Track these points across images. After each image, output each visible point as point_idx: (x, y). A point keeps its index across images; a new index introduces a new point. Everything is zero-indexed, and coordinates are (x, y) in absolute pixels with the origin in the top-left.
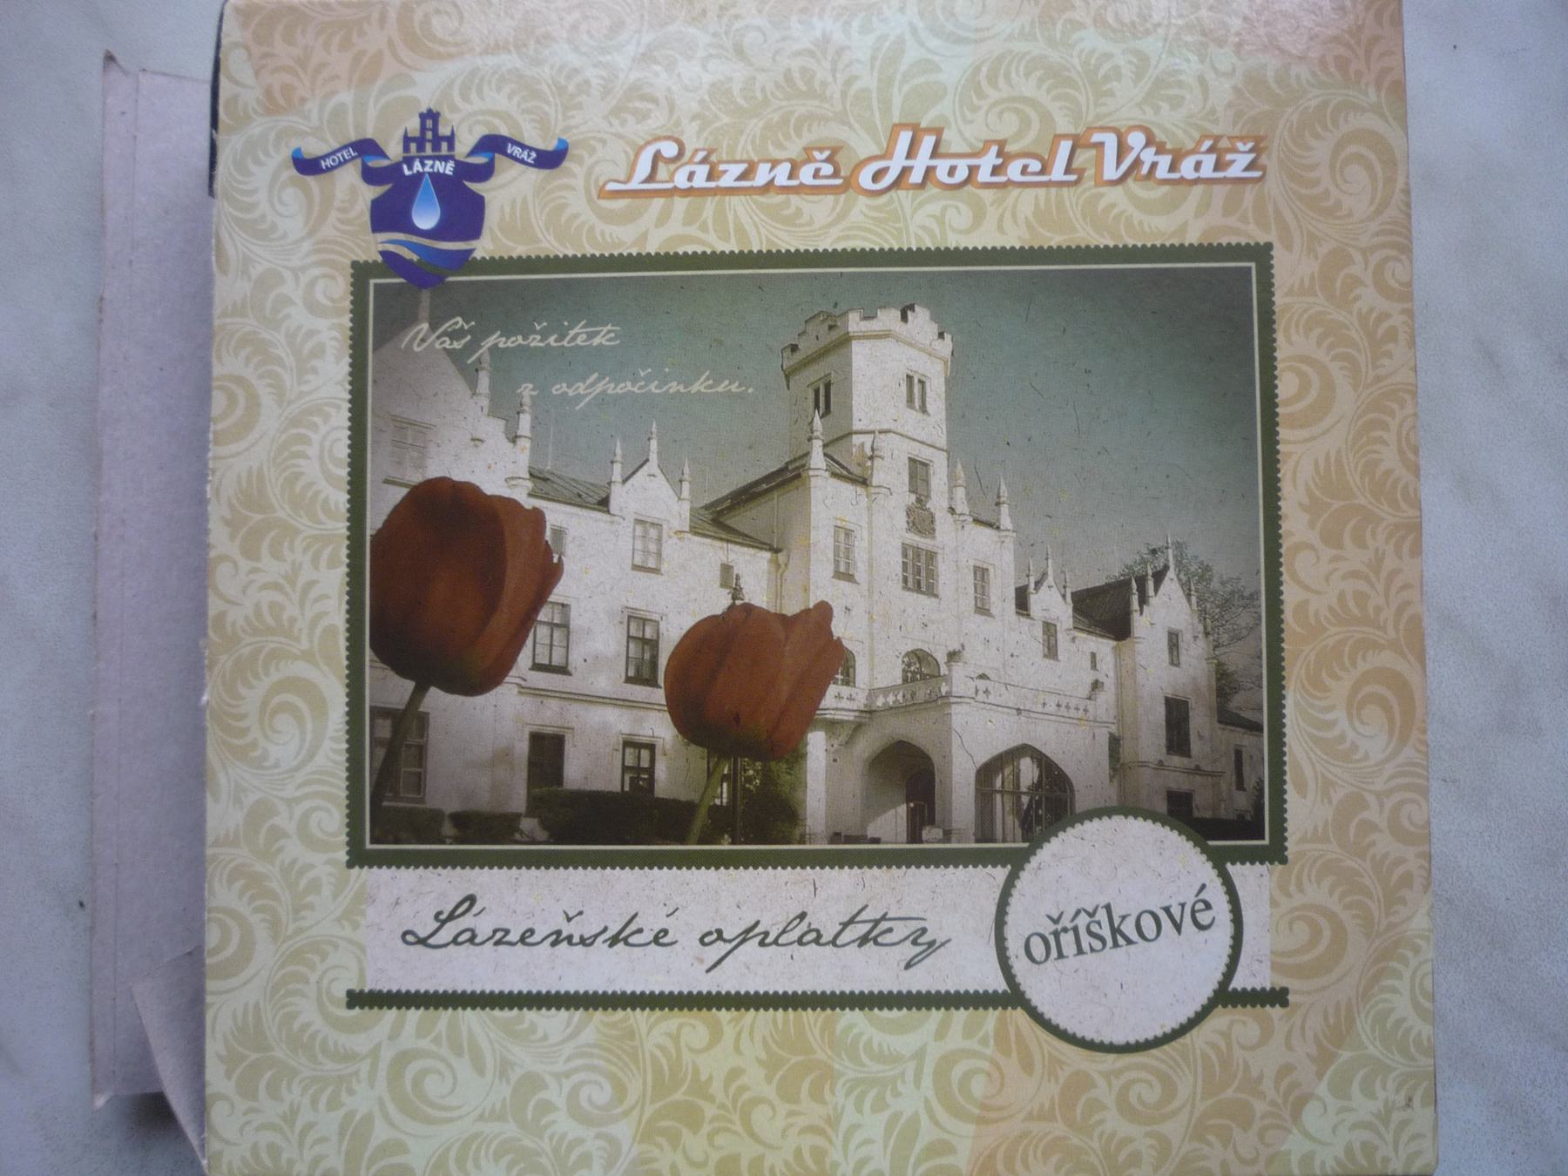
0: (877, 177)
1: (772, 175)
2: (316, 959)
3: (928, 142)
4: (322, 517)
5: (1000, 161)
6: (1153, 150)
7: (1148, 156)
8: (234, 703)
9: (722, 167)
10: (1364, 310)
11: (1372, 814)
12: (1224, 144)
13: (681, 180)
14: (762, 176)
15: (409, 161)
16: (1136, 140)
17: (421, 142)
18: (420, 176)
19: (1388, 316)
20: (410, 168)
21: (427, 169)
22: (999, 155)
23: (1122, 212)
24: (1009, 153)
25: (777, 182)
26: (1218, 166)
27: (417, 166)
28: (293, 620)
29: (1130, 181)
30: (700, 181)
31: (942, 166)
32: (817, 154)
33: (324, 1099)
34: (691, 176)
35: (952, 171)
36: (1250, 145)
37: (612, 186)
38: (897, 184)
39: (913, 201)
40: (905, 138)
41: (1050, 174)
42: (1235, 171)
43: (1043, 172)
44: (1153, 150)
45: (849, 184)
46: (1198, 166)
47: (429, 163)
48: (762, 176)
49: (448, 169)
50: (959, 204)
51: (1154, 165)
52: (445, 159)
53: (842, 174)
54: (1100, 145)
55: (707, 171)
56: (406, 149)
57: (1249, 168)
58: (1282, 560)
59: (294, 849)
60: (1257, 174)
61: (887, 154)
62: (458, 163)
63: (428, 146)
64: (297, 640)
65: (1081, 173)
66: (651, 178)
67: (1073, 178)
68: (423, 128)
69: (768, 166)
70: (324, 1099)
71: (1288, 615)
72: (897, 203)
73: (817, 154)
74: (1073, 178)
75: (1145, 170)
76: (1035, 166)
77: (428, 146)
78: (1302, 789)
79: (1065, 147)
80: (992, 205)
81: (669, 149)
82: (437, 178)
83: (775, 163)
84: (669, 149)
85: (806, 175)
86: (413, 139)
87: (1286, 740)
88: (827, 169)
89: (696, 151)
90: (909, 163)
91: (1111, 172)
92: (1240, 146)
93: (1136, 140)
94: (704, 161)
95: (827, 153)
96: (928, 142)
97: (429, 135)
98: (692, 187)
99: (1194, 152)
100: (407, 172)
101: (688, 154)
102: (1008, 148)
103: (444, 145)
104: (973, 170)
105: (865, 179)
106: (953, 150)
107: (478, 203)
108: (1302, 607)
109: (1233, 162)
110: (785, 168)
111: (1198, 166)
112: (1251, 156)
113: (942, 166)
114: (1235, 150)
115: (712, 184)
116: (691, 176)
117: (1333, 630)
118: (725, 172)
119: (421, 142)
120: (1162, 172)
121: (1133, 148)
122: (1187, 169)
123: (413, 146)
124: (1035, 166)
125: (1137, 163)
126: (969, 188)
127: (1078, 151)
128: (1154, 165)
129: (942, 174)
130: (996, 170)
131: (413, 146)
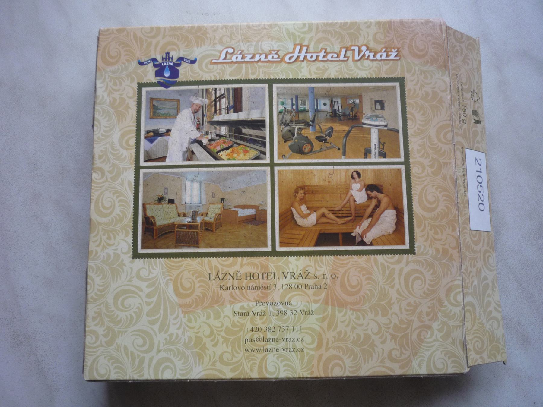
0: (290, 59)
1: (260, 58)
2: (417, 131)
3: (305, 49)
4: (424, 262)
5: (325, 54)
6: (368, 51)
7: (367, 53)
8: (447, 205)
9: (246, 55)
10: (103, 327)
11: (109, 176)
12: (389, 50)
13: (234, 59)
14: (257, 58)
15: (163, 63)
16: (364, 48)
17: (166, 59)
18: (165, 66)
19: (96, 325)
20: (163, 64)
21: (167, 64)
22: (325, 52)
23: (176, 358)
24: (328, 52)
25: (262, 60)
26: (387, 56)
27: (165, 64)
28: (431, 229)
29: (362, 60)
30: (239, 59)
31: (309, 56)
32: (273, 52)
33: (412, 92)
34: (237, 58)
35: (312, 57)
36: (396, 50)
37: (214, 61)
38: (296, 60)
39: (242, 362)
40: (298, 48)
41: (339, 58)
42: (392, 57)
43: (337, 57)
44: (368, 51)
45: (282, 60)
46: (381, 56)
47: (167, 63)
48: (257, 58)
49: (172, 64)
50: (227, 361)
51: (369, 56)
52: (171, 62)
53: (280, 57)
54: (354, 50)
55: (241, 57)
56: (163, 60)
57: (396, 56)
58: (132, 250)
59: (426, 162)
60: (398, 58)
61: (293, 52)
62: (173, 63)
63: (167, 60)
64: (429, 224)
65: (348, 58)
66: (225, 59)
67: (346, 59)
68: (166, 56)
69: (259, 55)
70: (412, 92)
71: (131, 233)
72: (247, 361)
73: (273, 52)
74: (346, 59)
75: (366, 57)
76: (335, 55)
77: (167, 60)
78: (129, 182)
79: (344, 51)
80: (217, 361)
81: (230, 50)
82: (169, 66)
83: (261, 54)
84: (230, 50)
85: (270, 58)
86: (164, 58)
87: (133, 197)
88: (276, 56)
89: (238, 51)
90: (299, 55)
91: (357, 57)
92: (393, 50)
93: (364, 48)
94: (240, 54)
95: (276, 52)
96: (305, 49)
97: (168, 57)
98: (237, 61)
99: (380, 52)
100: (163, 65)
101: (236, 52)
102: (328, 51)
103: (171, 59)
104: (317, 57)
105: (287, 59)
106: (311, 51)
107: (178, 71)
108: (126, 236)
109: (391, 55)
110: (264, 56)
111: (381, 56)
112: (397, 53)
113: (309, 56)
114: (391, 51)
115: (243, 60)
116: (237, 58)
117: (117, 229)
118: (246, 57)
119: (166, 59)
120: (371, 57)
121: (363, 51)
122: (378, 57)
123: (164, 60)
124: (335, 55)
125: (364, 55)
126: (316, 62)
127: (347, 52)
128: (369, 56)
129: (309, 58)
130: (324, 57)
131: (164, 60)
